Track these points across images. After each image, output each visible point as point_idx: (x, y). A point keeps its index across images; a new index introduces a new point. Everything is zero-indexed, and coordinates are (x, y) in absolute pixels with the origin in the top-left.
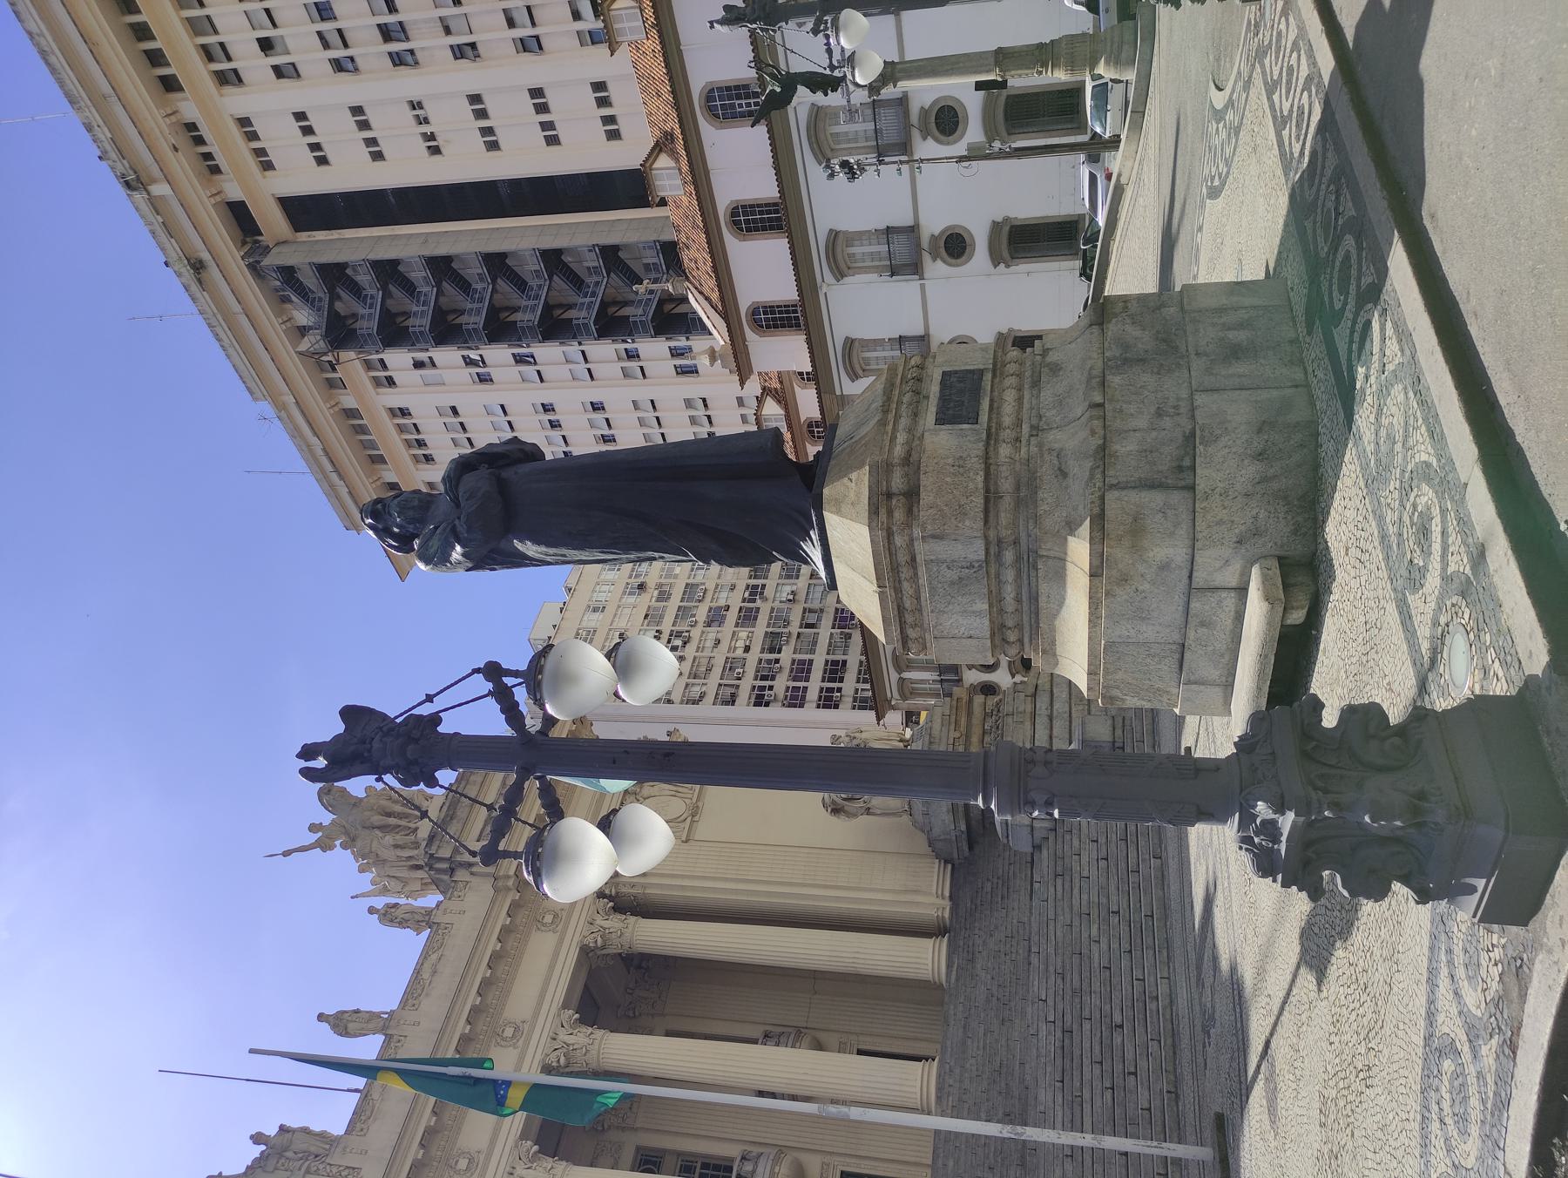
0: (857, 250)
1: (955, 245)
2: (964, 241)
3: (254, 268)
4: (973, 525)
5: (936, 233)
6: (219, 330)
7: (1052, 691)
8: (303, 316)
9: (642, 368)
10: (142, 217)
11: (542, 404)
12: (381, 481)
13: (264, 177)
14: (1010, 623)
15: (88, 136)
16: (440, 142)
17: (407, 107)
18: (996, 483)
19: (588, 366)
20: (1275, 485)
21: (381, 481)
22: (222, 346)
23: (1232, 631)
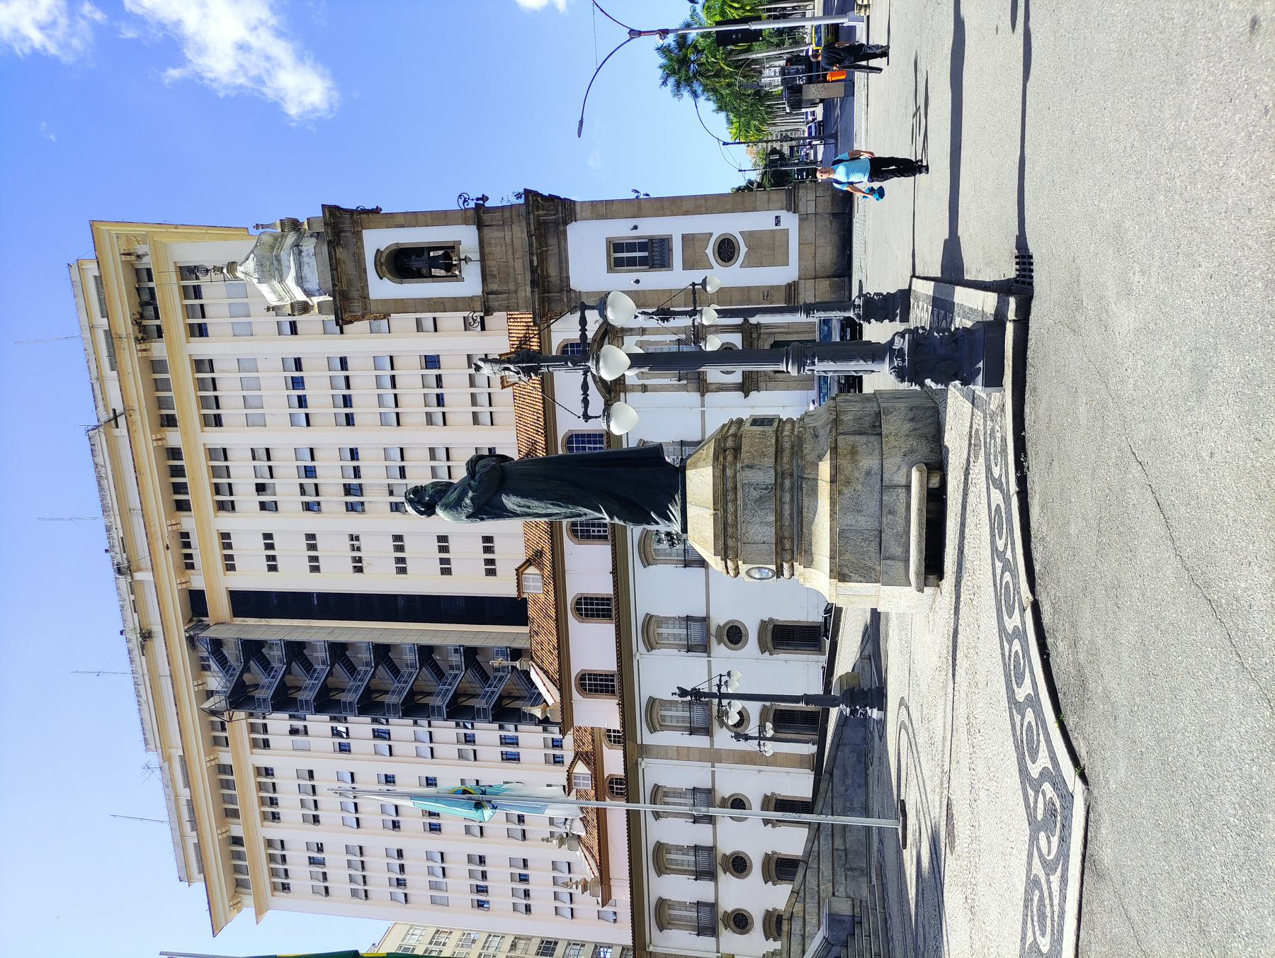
0: (662, 631)
1: (734, 635)
2: (741, 638)
3: (192, 641)
4: (769, 461)
5: (722, 625)
6: (142, 688)
7: (804, 918)
8: (215, 681)
9: (475, 751)
10: (119, 595)
11: (386, 775)
12: (228, 834)
13: (225, 575)
14: (786, 534)
15: (105, 535)
16: (364, 564)
17: (347, 538)
18: (781, 445)
19: (432, 745)
20: (920, 432)
21: (228, 834)
22: (139, 701)
23: (906, 517)
